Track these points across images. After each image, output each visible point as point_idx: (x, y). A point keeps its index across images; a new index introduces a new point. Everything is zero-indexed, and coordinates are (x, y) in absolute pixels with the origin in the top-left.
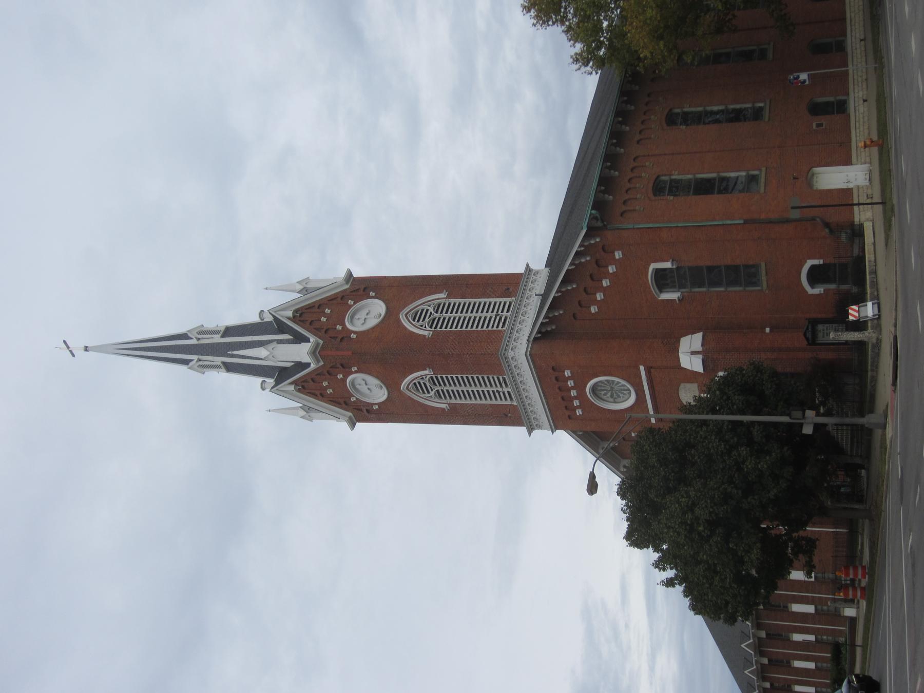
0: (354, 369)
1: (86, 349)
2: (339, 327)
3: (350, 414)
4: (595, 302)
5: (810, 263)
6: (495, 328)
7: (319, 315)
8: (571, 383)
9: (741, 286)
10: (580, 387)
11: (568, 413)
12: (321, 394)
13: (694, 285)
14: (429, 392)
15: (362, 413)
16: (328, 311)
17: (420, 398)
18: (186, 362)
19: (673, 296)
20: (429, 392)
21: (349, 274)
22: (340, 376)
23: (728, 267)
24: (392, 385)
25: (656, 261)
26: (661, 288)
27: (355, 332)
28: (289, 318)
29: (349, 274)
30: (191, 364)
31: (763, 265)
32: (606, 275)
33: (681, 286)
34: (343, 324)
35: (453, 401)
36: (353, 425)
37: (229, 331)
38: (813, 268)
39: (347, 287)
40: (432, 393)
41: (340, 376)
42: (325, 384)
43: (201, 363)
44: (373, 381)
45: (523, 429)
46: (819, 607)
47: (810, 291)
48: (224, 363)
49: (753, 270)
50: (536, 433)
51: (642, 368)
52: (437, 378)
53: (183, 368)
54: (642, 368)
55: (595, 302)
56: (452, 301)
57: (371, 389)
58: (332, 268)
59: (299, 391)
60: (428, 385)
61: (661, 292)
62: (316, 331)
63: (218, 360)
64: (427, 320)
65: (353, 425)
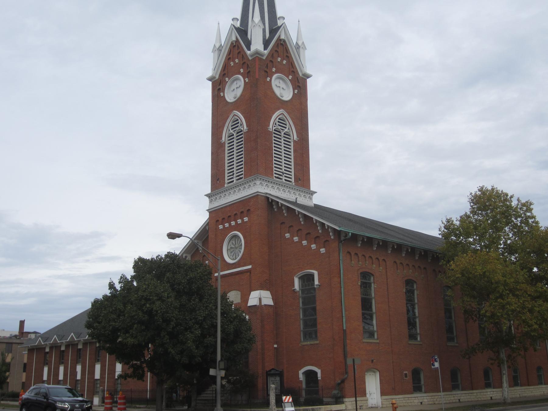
0: (247, 80)
2: (274, 70)
3: (217, 77)
4: (292, 236)
5: (319, 371)
7: (282, 56)
9: (303, 329)
14: (232, 129)
16: (285, 62)
20: (232, 129)
21: (309, 76)
22: (242, 70)
23: (315, 320)
24: (237, 105)
27: (271, 80)
29: (309, 76)
32: (310, 243)
33: (303, 291)
34: (276, 72)
35: (227, 145)
36: (210, 79)
40: (231, 131)
41: (242, 70)
42: (237, 61)
45: (209, 191)
47: (301, 372)
49: (314, 336)
50: (207, 198)
51: (250, 267)
54: (250, 267)
56: (292, 144)
57: (234, 91)
60: (237, 128)
64: (279, 127)
65: (210, 79)
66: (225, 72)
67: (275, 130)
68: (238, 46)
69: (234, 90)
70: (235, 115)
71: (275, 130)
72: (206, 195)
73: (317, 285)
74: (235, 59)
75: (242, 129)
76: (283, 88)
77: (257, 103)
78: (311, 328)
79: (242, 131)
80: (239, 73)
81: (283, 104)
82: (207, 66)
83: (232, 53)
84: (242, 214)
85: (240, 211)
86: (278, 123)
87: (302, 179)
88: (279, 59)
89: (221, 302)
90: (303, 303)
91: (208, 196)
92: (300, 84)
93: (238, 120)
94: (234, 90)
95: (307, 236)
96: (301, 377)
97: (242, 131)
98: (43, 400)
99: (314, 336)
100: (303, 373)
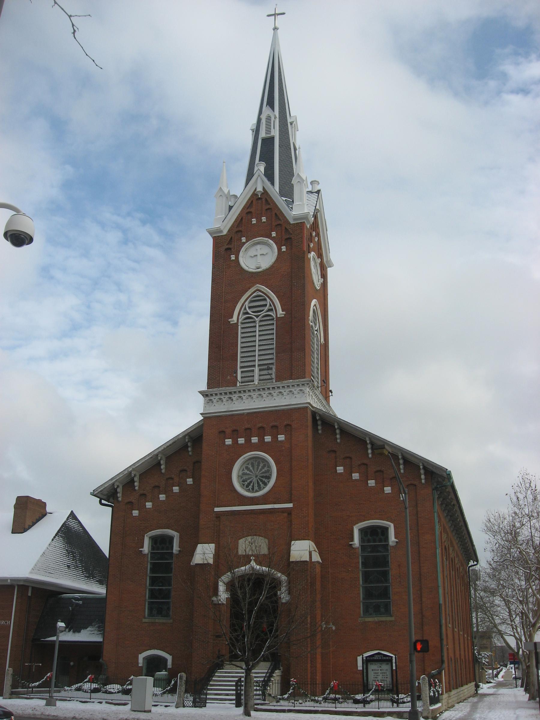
0: (284, 249)
1: (275, 29)
3: (225, 232)
4: (349, 471)
5: (169, 658)
8: (268, 439)
9: (364, 599)
10: (262, 446)
11: (228, 431)
13: (154, 565)
15: (225, 247)
17: (244, 302)
19: (146, 548)
22: (274, 234)
23: (386, 589)
25: (181, 538)
26: (155, 540)
31: (393, 619)
32: (382, 484)
33: (363, 548)
38: (166, 660)
41: (274, 234)
45: (204, 387)
47: (141, 657)
49: (382, 610)
50: (201, 398)
51: (290, 505)
54: (290, 505)
55: (349, 471)
61: (150, 538)
68: (266, 200)
72: (200, 392)
73: (393, 542)
78: (378, 596)
80: (269, 236)
84: (275, 431)
85: (271, 424)
87: (326, 393)
88: (254, 221)
90: (362, 562)
91: (204, 394)
95: (379, 475)
99: (382, 610)
100: (144, 658)
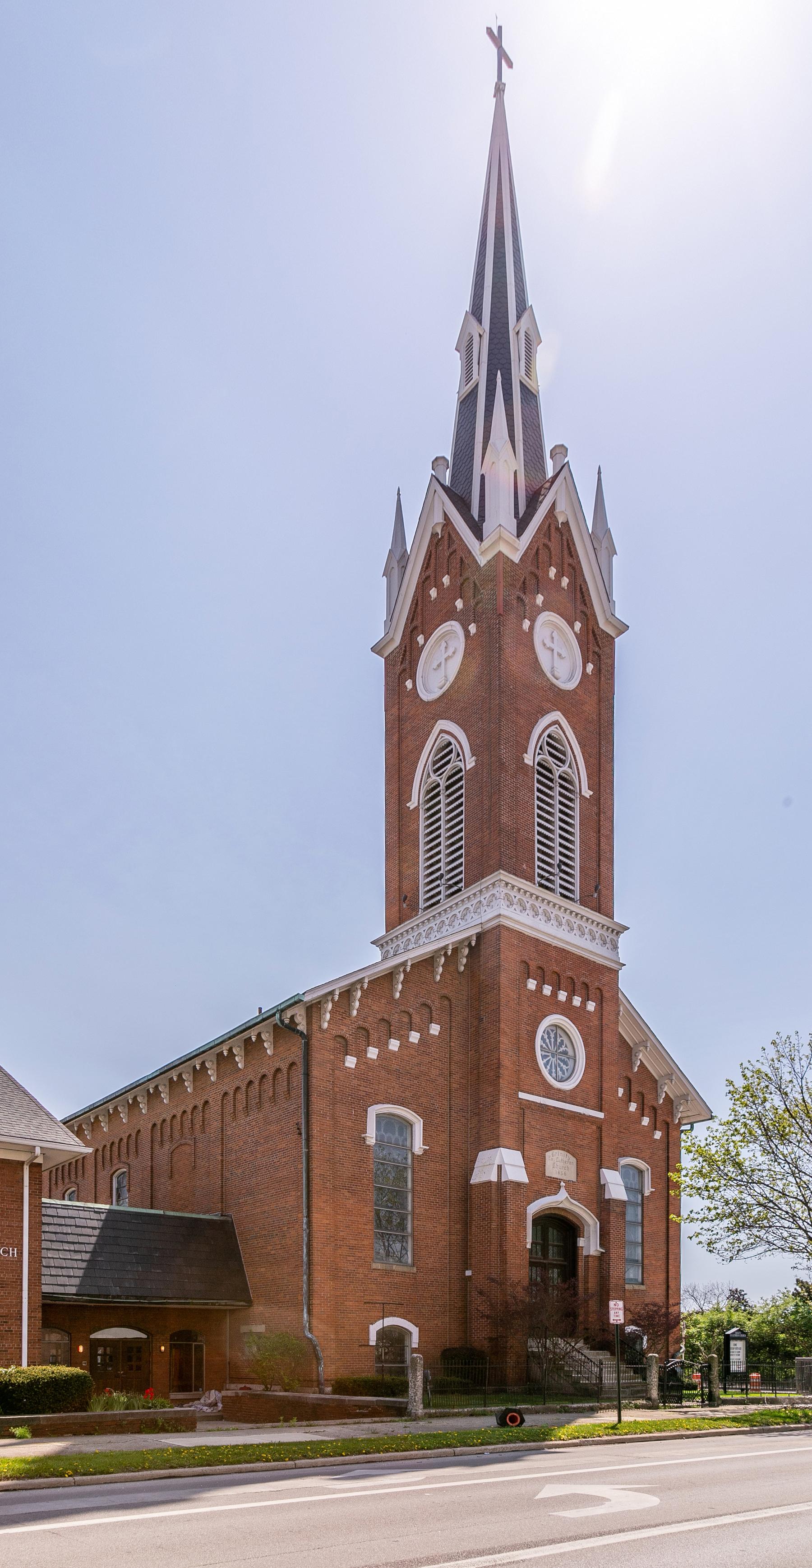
2: (540, 599)
6: (537, 870)
7: (561, 563)
12: (415, 628)
14: (435, 771)
16: (565, 581)
18: (476, 311)
20: (435, 771)
21: (623, 628)
24: (445, 706)
27: (532, 628)
28: (553, 506)
29: (623, 628)
30: (473, 321)
34: (546, 607)
35: (422, 815)
36: (377, 649)
37: (530, 396)
39: (502, 871)
40: (434, 777)
42: (446, 580)
43: (476, 339)
44: (453, 667)
45: (381, 931)
46: (241, 1072)
48: (474, 392)
52: (460, 779)
53: (466, 306)
56: (577, 805)
57: (444, 659)
58: (629, 592)
59: (434, 535)
60: (449, 766)
62: (534, 554)
63: (480, 376)
64: (550, 759)
65: (377, 649)
66: (415, 623)
67: (539, 764)
69: (439, 665)
70: (442, 731)
71: (539, 764)
74: (440, 579)
75: (462, 765)
76: (559, 655)
77: (498, 695)
79: (460, 770)
81: (559, 699)
82: (369, 612)
83: (433, 561)
86: (546, 747)
89: (67, 1528)
92: (597, 646)
93: (450, 744)
94: (439, 665)
96: (374, 1329)
97: (460, 770)
98: (65, 1370)
